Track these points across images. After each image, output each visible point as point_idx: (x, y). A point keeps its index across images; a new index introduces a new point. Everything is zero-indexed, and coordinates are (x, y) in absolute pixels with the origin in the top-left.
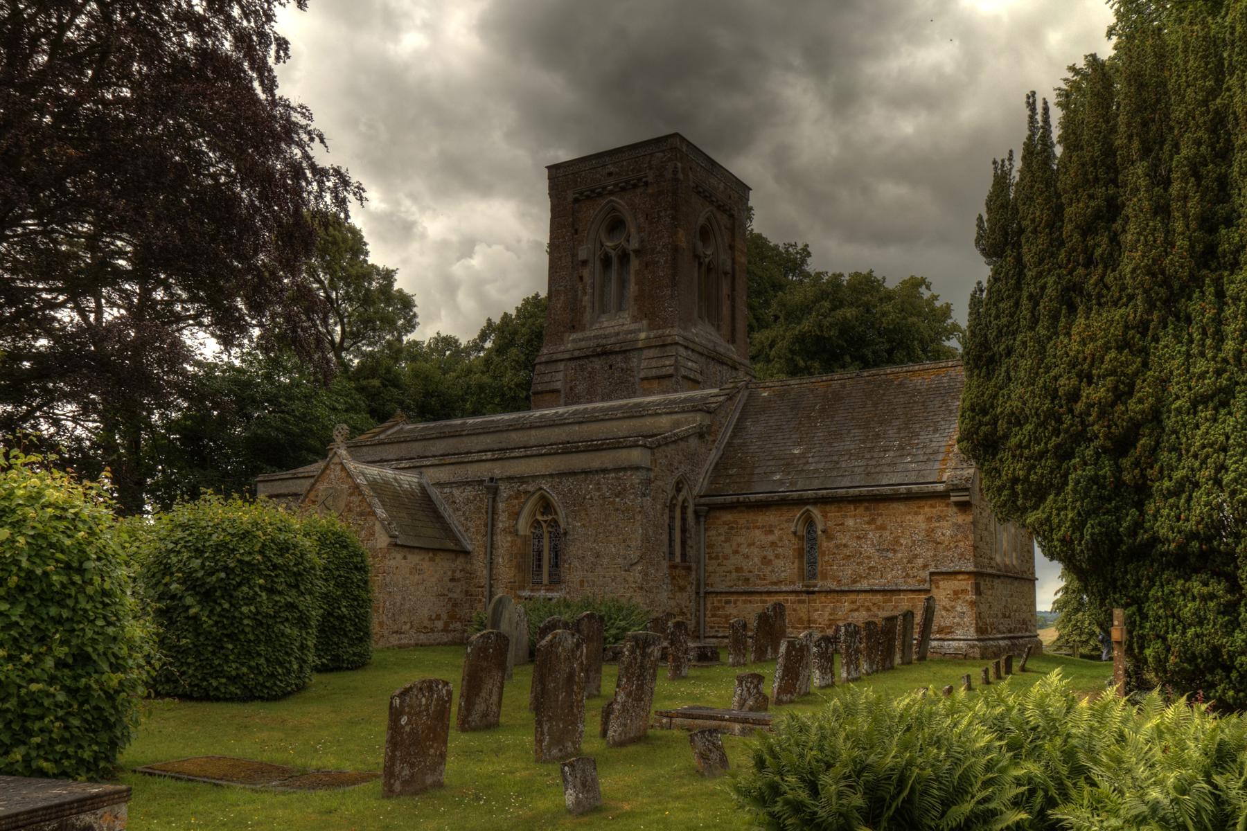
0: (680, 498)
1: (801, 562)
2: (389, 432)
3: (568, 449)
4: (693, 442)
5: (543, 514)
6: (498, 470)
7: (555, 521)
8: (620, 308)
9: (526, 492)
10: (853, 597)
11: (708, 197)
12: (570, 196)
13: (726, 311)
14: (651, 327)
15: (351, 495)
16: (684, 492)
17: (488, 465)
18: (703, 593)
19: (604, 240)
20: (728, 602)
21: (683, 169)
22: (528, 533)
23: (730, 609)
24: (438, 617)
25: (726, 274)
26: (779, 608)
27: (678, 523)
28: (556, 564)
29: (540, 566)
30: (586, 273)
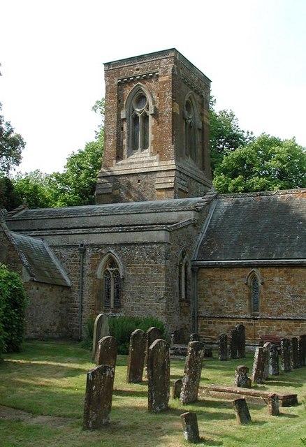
0: (184, 261)
1: (250, 301)
2: (20, 213)
3: (126, 228)
4: (190, 228)
5: (110, 267)
6: (86, 240)
7: (117, 271)
8: (145, 146)
9: (102, 254)
10: (279, 322)
11: (190, 86)
12: (116, 81)
13: (199, 151)
14: (161, 159)
15: (9, 250)
16: (186, 257)
17: (80, 236)
18: (196, 318)
19: (134, 107)
20: (210, 323)
21: (177, 68)
22: (102, 278)
23: (211, 327)
24: (55, 324)
25: (199, 129)
26: (242, 328)
27: (183, 275)
28: (118, 296)
29: (109, 297)
30: (125, 126)
